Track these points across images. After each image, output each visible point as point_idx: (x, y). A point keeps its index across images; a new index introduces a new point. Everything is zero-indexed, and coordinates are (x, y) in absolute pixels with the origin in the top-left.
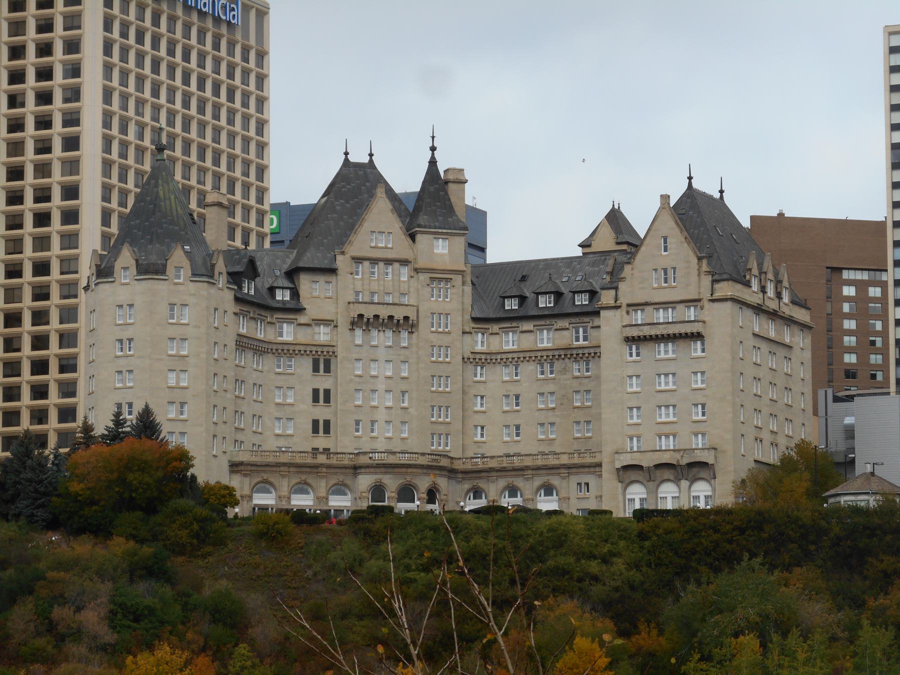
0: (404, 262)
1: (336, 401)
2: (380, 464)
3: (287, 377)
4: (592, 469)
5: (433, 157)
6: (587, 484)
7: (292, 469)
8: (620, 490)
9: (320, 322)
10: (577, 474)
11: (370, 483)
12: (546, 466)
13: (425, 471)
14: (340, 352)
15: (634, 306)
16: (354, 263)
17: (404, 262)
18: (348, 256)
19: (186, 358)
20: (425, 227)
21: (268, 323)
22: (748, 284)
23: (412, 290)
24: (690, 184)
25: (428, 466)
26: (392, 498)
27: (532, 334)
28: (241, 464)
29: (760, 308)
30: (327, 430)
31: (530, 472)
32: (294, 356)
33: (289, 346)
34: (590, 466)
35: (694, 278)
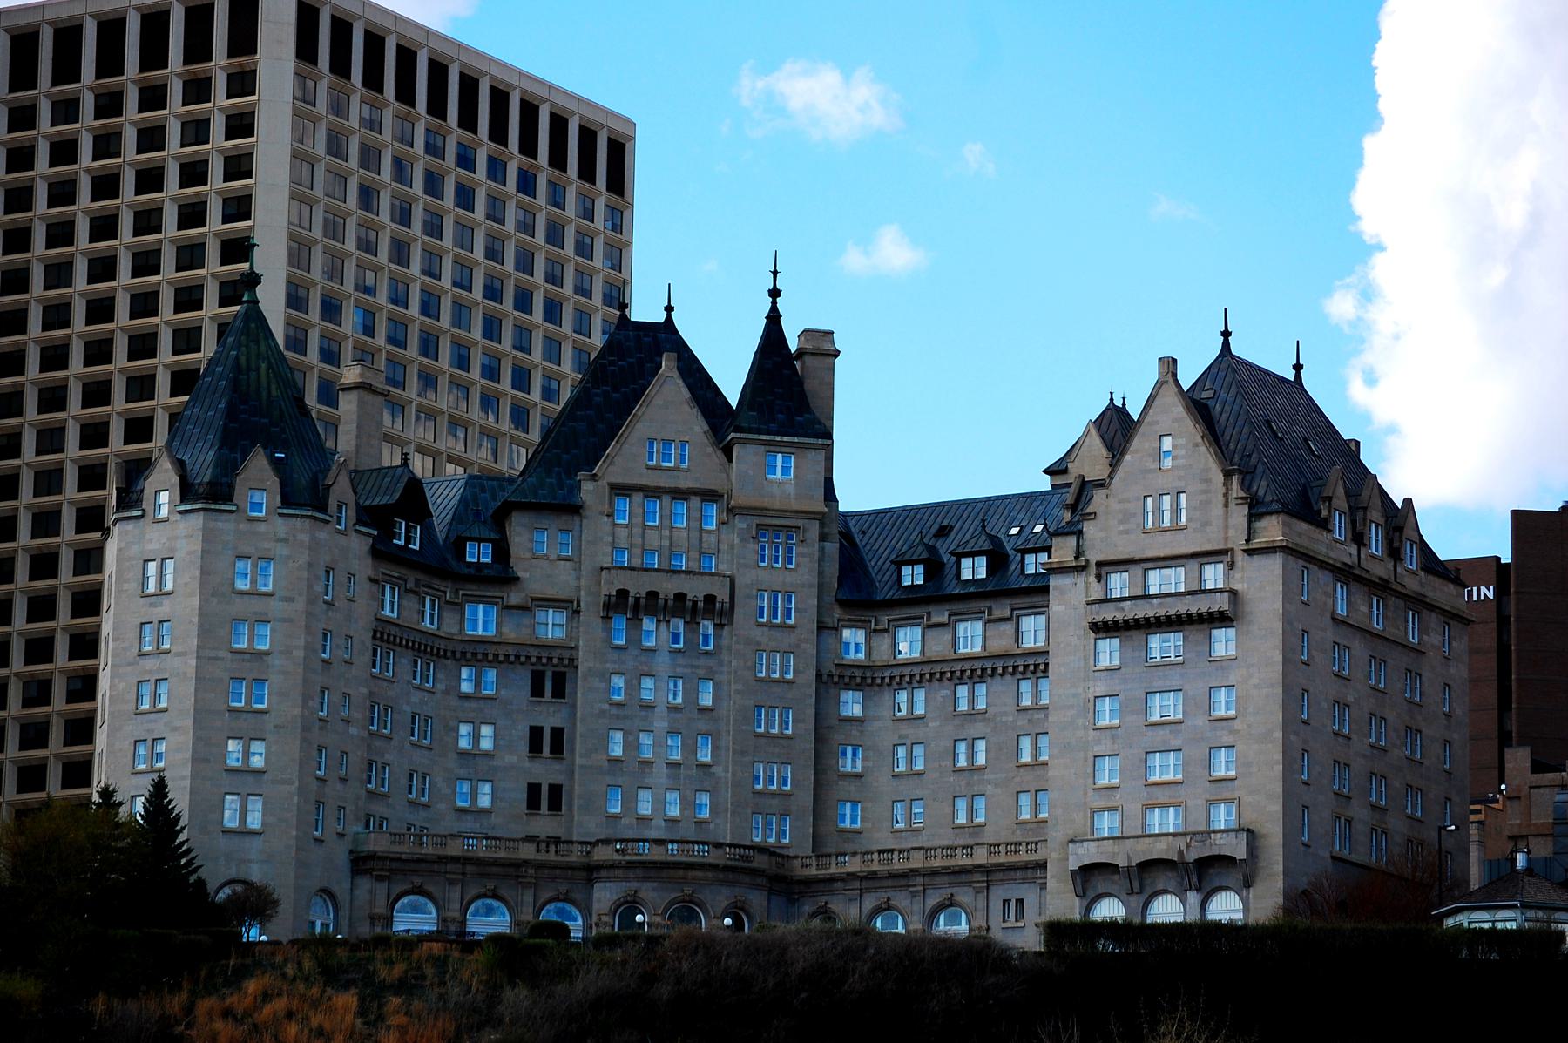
0: (709, 496)
1: (573, 751)
3: (482, 704)
4: (1030, 874)
5: (774, 308)
6: (1020, 902)
7: (469, 868)
10: (1002, 882)
11: (615, 898)
12: (949, 868)
13: (721, 876)
14: (585, 662)
15: (1106, 567)
17: (709, 496)
18: (603, 483)
19: (265, 658)
20: (750, 431)
21: (447, 602)
22: (1324, 525)
23: (724, 547)
24: (1226, 345)
27: (946, 630)
28: (372, 856)
29: (1349, 572)
30: (555, 805)
33: (487, 646)
34: (1026, 867)
35: (1217, 510)
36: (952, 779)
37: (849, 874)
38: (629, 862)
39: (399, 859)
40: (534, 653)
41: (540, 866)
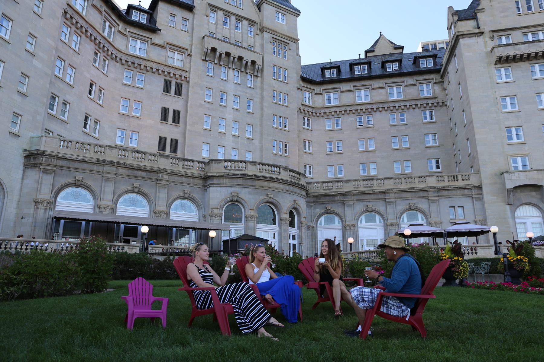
2: (237, 175)
3: (135, 90)
7: (121, 171)
8: (509, 214)
9: (175, 47)
10: (448, 196)
11: (223, 197)
12: (413, 188)
14: (193, 80)
16: (209, 9)
21: (119, 32)
25: (291, 182)
26: (252, 217)
31: (392, 195)
32: (145, 72)
36: (358, 156)
37: (346, 192)
38: (234, 174)
39: (65, 159)
40: (167, 70)
41: (172, 174)
